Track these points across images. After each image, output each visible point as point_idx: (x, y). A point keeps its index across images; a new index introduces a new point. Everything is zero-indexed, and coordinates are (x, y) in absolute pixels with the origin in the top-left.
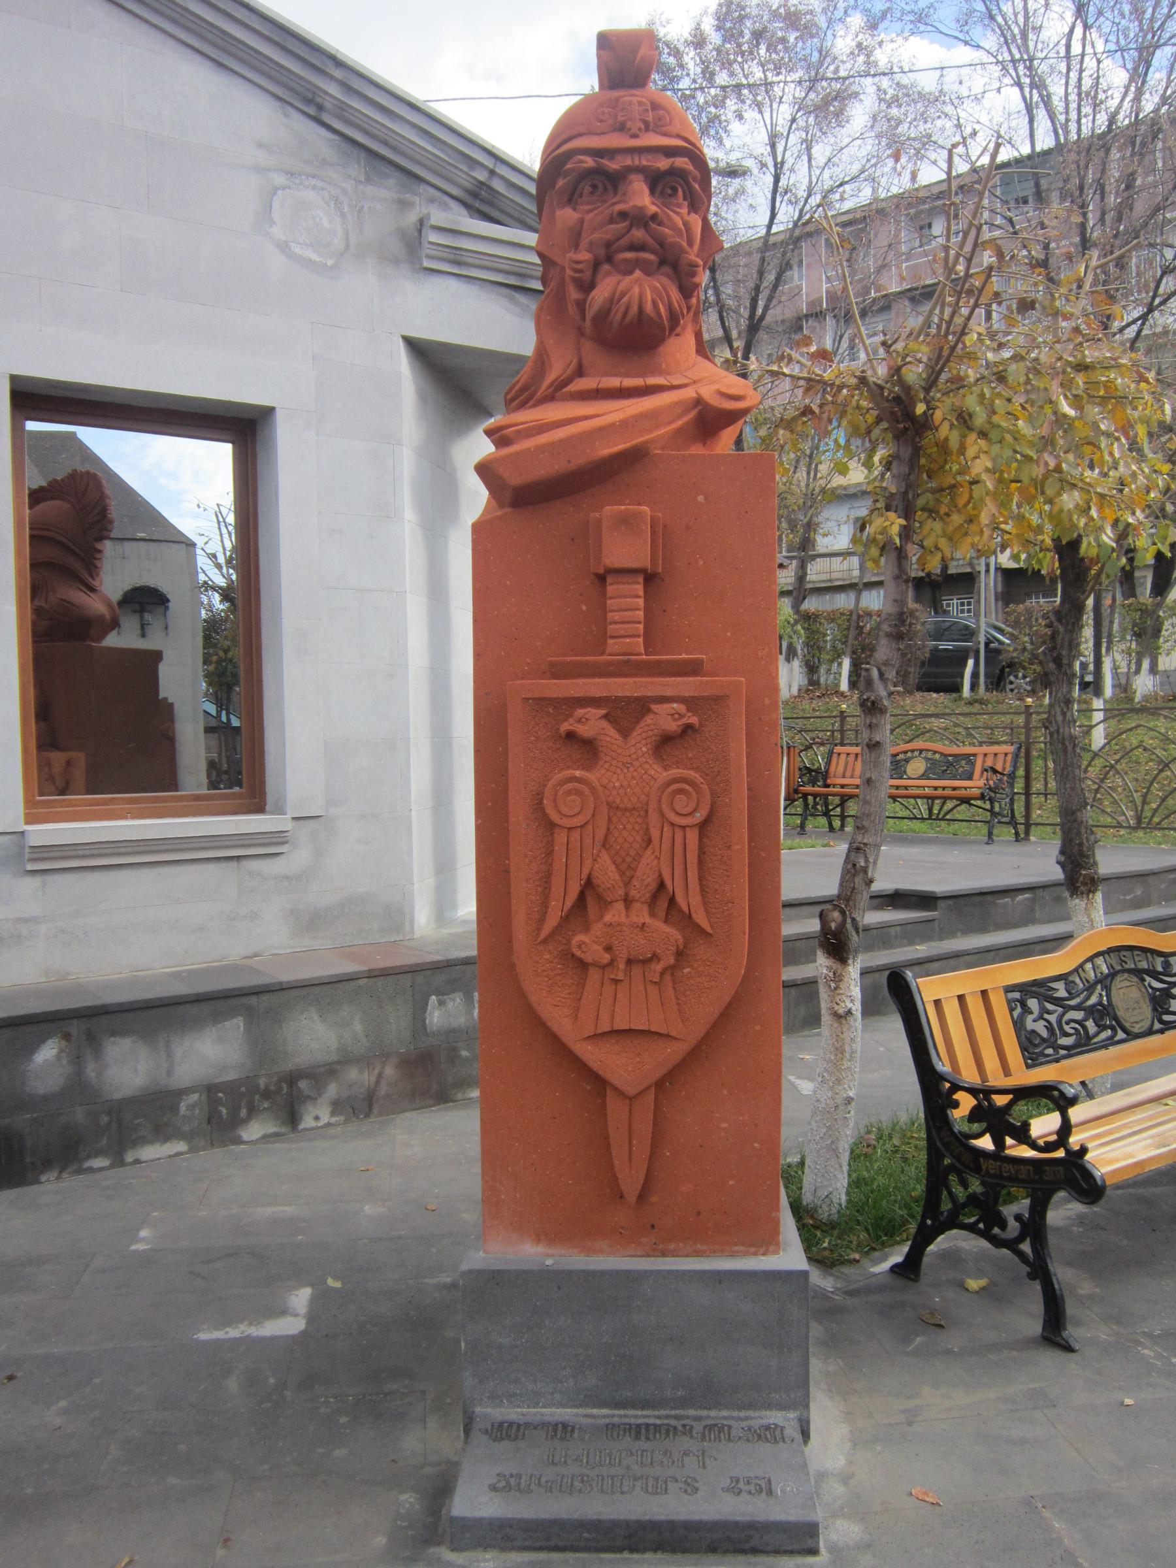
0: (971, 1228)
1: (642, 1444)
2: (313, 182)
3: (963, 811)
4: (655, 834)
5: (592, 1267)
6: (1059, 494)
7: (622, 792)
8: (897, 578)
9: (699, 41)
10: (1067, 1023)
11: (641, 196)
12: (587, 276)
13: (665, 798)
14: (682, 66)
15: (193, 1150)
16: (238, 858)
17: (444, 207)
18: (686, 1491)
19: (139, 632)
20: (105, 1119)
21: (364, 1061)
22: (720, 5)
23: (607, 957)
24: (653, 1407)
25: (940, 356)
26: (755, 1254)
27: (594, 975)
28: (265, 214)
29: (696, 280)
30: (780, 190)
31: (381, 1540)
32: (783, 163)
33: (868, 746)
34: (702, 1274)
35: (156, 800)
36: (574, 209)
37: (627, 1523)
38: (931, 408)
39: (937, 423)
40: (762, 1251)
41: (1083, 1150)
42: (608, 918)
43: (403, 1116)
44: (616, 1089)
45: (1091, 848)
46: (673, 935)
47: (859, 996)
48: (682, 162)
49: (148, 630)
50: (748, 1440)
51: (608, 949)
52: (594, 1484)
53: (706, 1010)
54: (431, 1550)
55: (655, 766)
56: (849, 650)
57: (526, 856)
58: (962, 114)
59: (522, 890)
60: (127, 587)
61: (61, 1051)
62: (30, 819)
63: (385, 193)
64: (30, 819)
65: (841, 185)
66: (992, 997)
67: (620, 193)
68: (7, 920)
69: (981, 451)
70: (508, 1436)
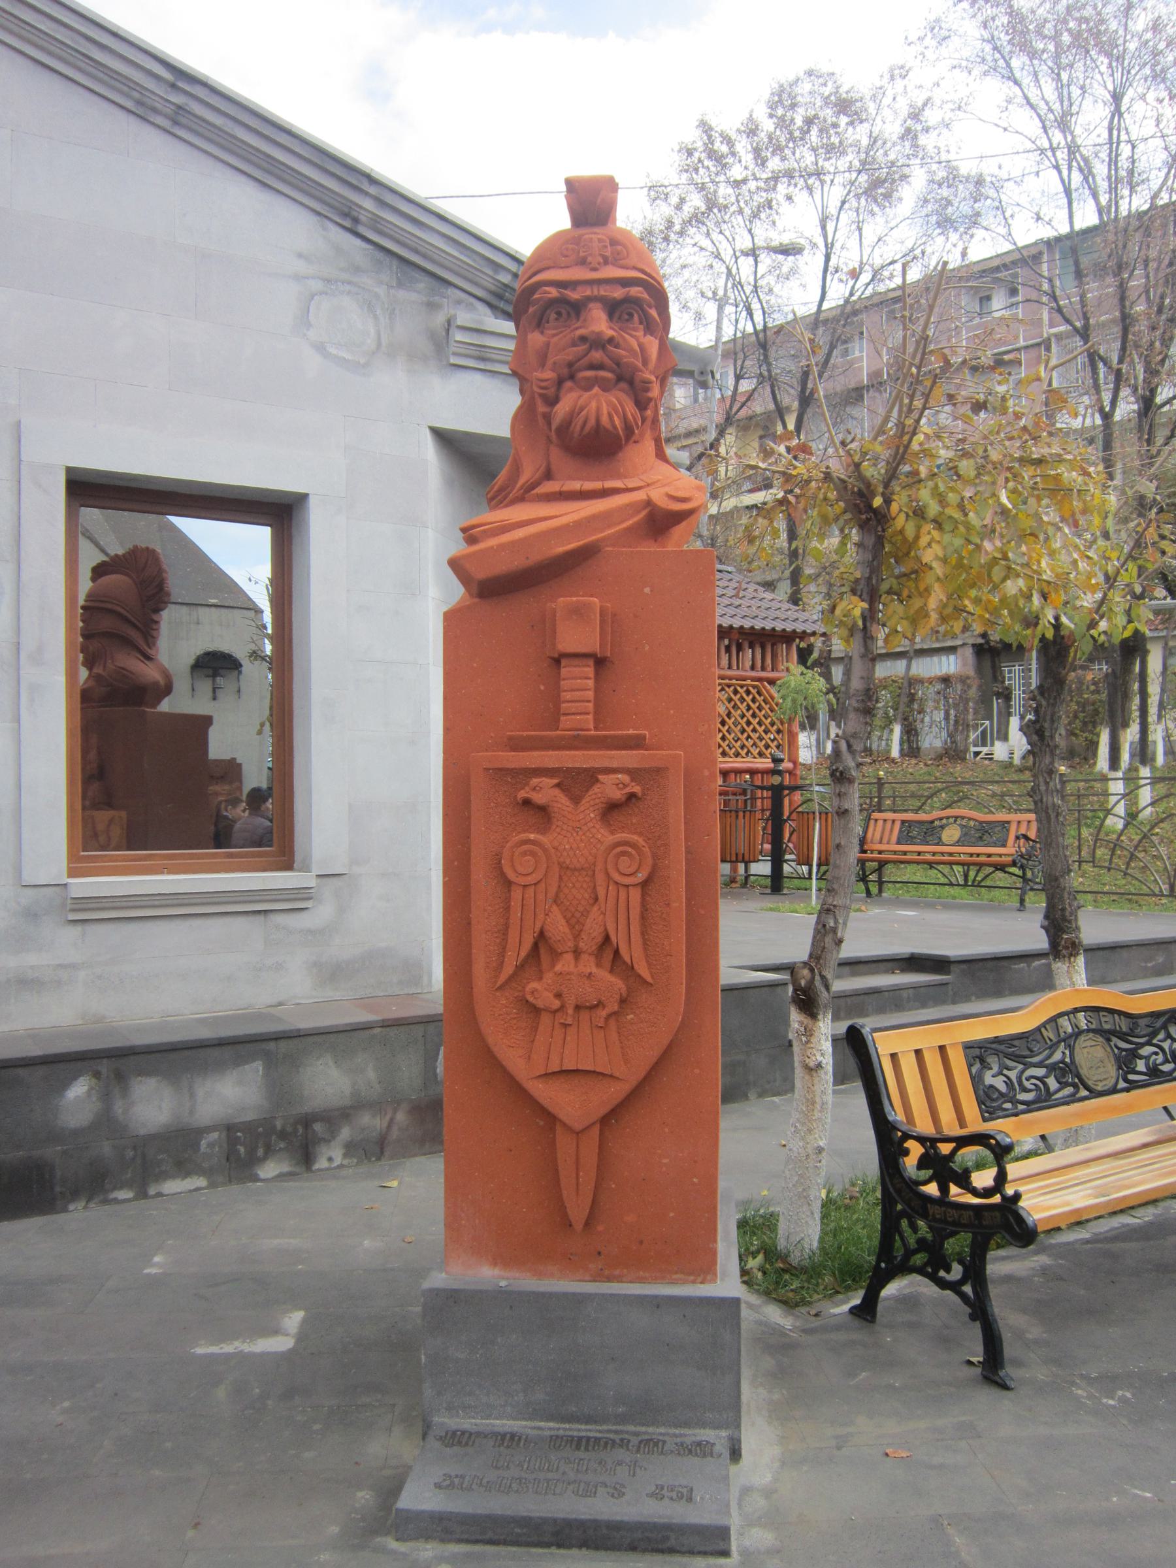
0: (920, 1271)
1: (581, 1454)
2: (348, 287)
3: (1000, 878)
4: (601, 892)
5: (542, 1289)
6: (1004, 580)
7: (571, 853)
8: (863, 656)
9: (752, 131)
10: (1027, 1079)
11: (599, 323)
12: (551, 392)
13: (611, 858)
14: (733, 154)
15: (212, 1185)
16: (266, 912)
17: (471, 308)
18: (613, 1496)
19: (210, 694)
20: (130, 1153)
21: (376, 1106)
22: (773, 94)
23: (557, 1004)
24: (596, 1422)
25: (897, 453)
26: (694, 1282)
27: (546, 1019)
28: (303, 320)
29: (650, 395)
30: (831, 269)
31: (335, 1529)
32: (832, 244)
33: (837, 813)
34: (641, 1300)
35: (192, 856)
36: (542, 333)
37: (555, 1520)
38: (888, 501)
39: (893, 515)
40: (700, 1279)
41: (1017, 1197)
42: (558, 968)
43: (413, 1160)
44: (564, 1124)
45: (1074, 913)
46: (618, 984)
47: (830, 1050)
48: (635, 291)
49: (219, 693)
50: (679, 1454)
51: (558, 996)
52: (530, 1486)
53: (645, 1054)
54: (378, 1539)
55: (602, 831)
56: (900, 716)
57: (485, 910)
58: (1003, 197)
59: (482, 939)
60: (199, 652)
61: (91, 1089)
62: (72, 873)
63: (414, 296)
64: (72, 873)
65: (890, 264)
66: (951, 1052)
67: (582, 318)
68: (48, 966)
69: (932, 540)
70: (460, 1443)
